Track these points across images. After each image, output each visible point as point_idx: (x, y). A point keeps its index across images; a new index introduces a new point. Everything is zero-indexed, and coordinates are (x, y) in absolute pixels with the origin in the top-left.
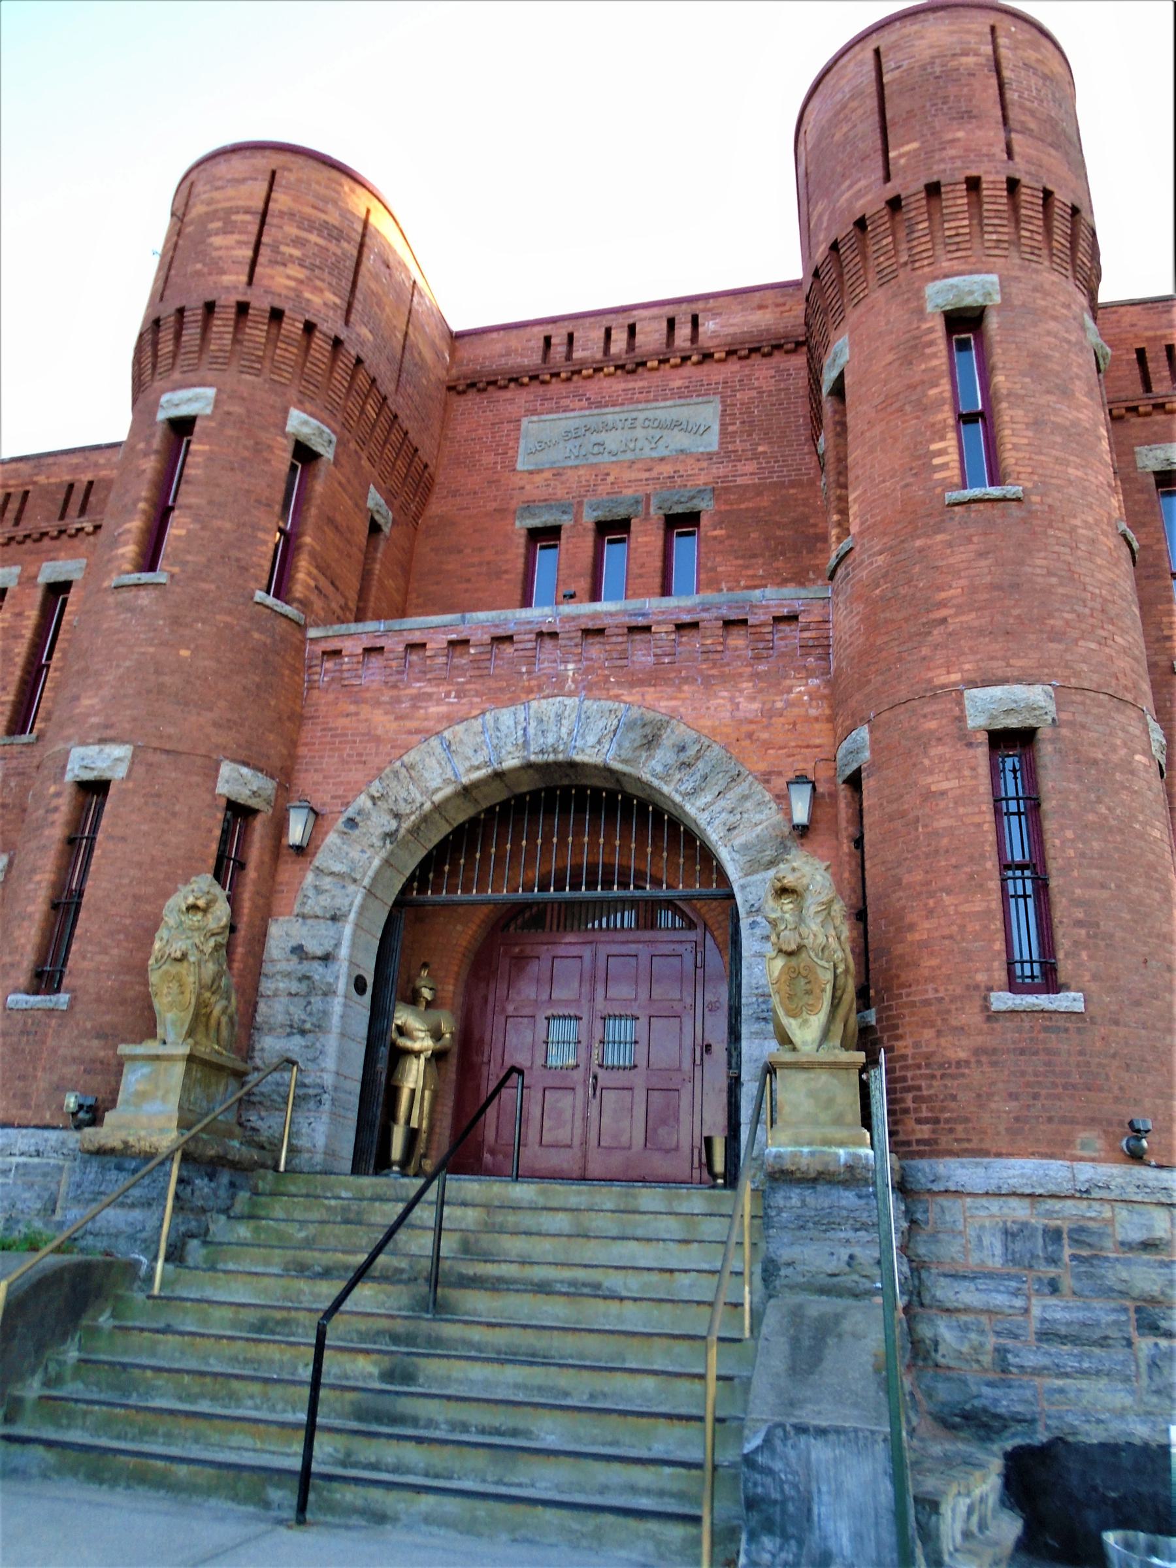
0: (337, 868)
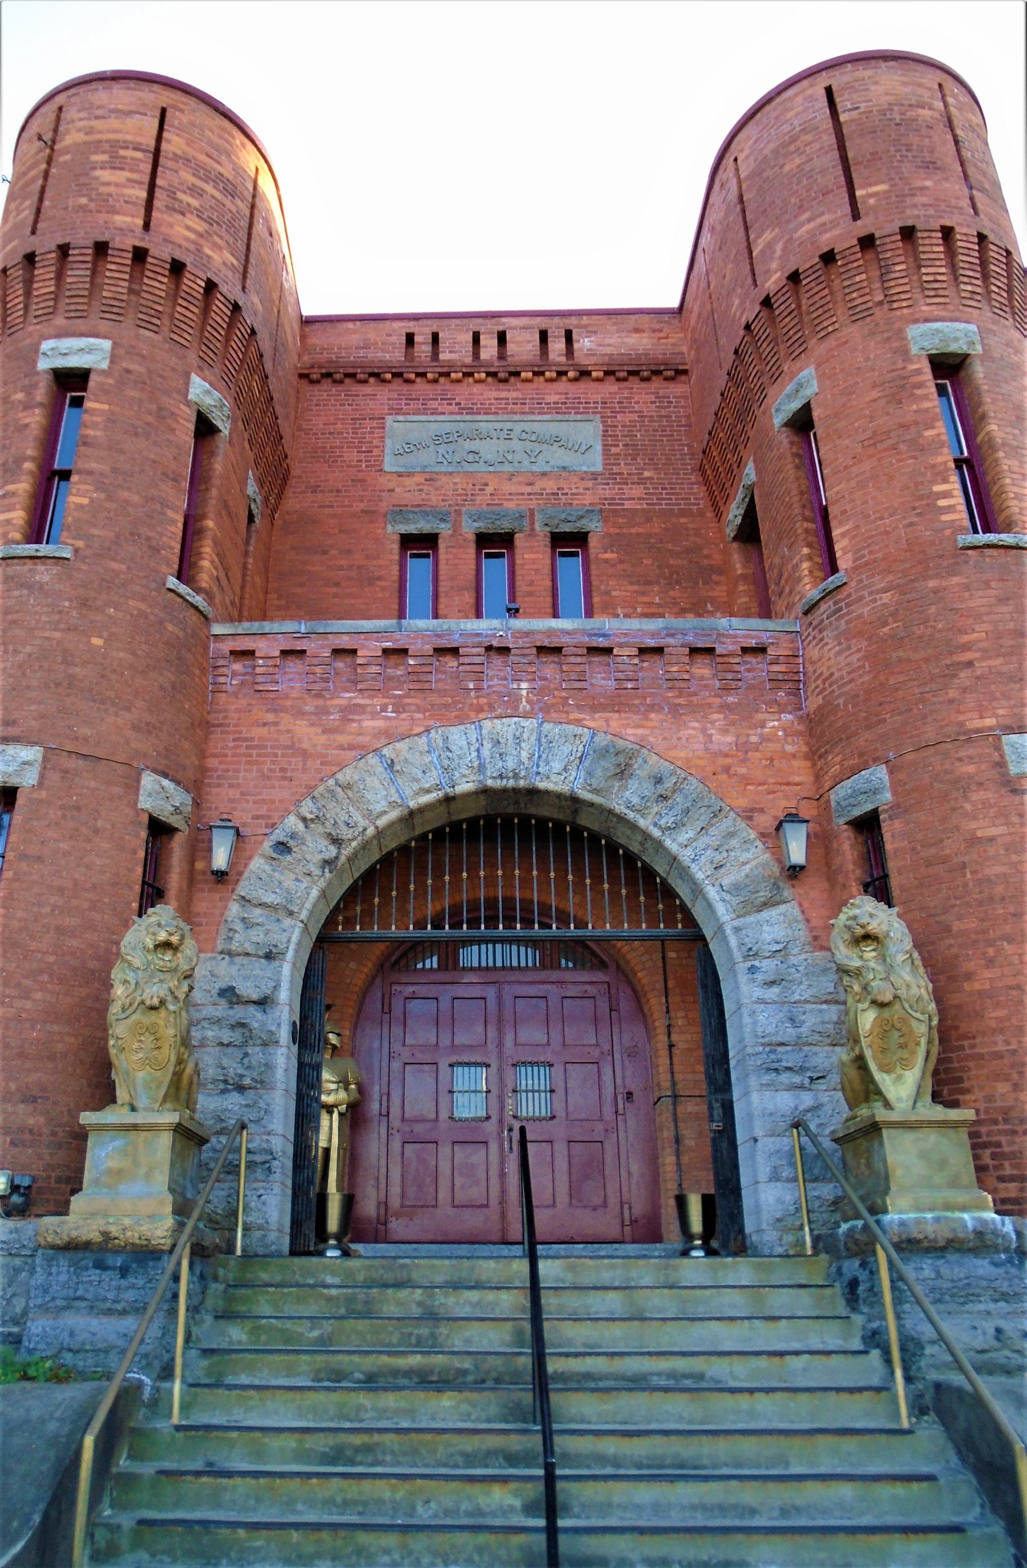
0: (270, 898)
